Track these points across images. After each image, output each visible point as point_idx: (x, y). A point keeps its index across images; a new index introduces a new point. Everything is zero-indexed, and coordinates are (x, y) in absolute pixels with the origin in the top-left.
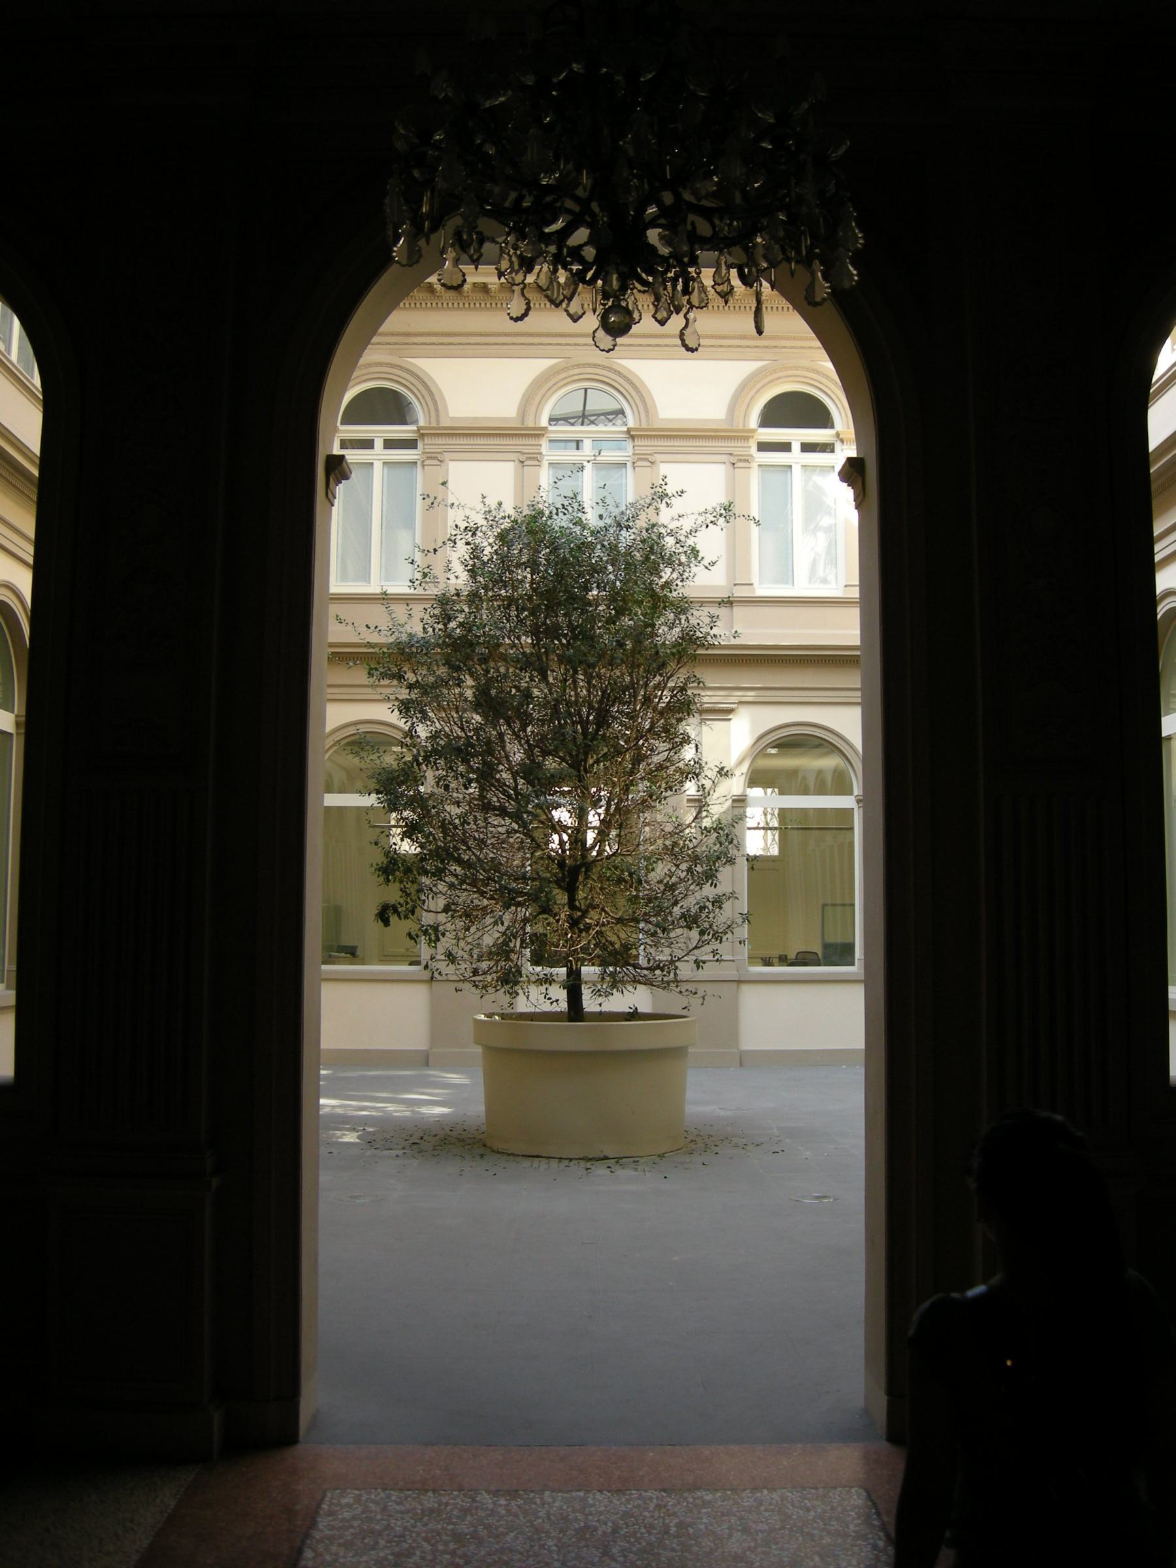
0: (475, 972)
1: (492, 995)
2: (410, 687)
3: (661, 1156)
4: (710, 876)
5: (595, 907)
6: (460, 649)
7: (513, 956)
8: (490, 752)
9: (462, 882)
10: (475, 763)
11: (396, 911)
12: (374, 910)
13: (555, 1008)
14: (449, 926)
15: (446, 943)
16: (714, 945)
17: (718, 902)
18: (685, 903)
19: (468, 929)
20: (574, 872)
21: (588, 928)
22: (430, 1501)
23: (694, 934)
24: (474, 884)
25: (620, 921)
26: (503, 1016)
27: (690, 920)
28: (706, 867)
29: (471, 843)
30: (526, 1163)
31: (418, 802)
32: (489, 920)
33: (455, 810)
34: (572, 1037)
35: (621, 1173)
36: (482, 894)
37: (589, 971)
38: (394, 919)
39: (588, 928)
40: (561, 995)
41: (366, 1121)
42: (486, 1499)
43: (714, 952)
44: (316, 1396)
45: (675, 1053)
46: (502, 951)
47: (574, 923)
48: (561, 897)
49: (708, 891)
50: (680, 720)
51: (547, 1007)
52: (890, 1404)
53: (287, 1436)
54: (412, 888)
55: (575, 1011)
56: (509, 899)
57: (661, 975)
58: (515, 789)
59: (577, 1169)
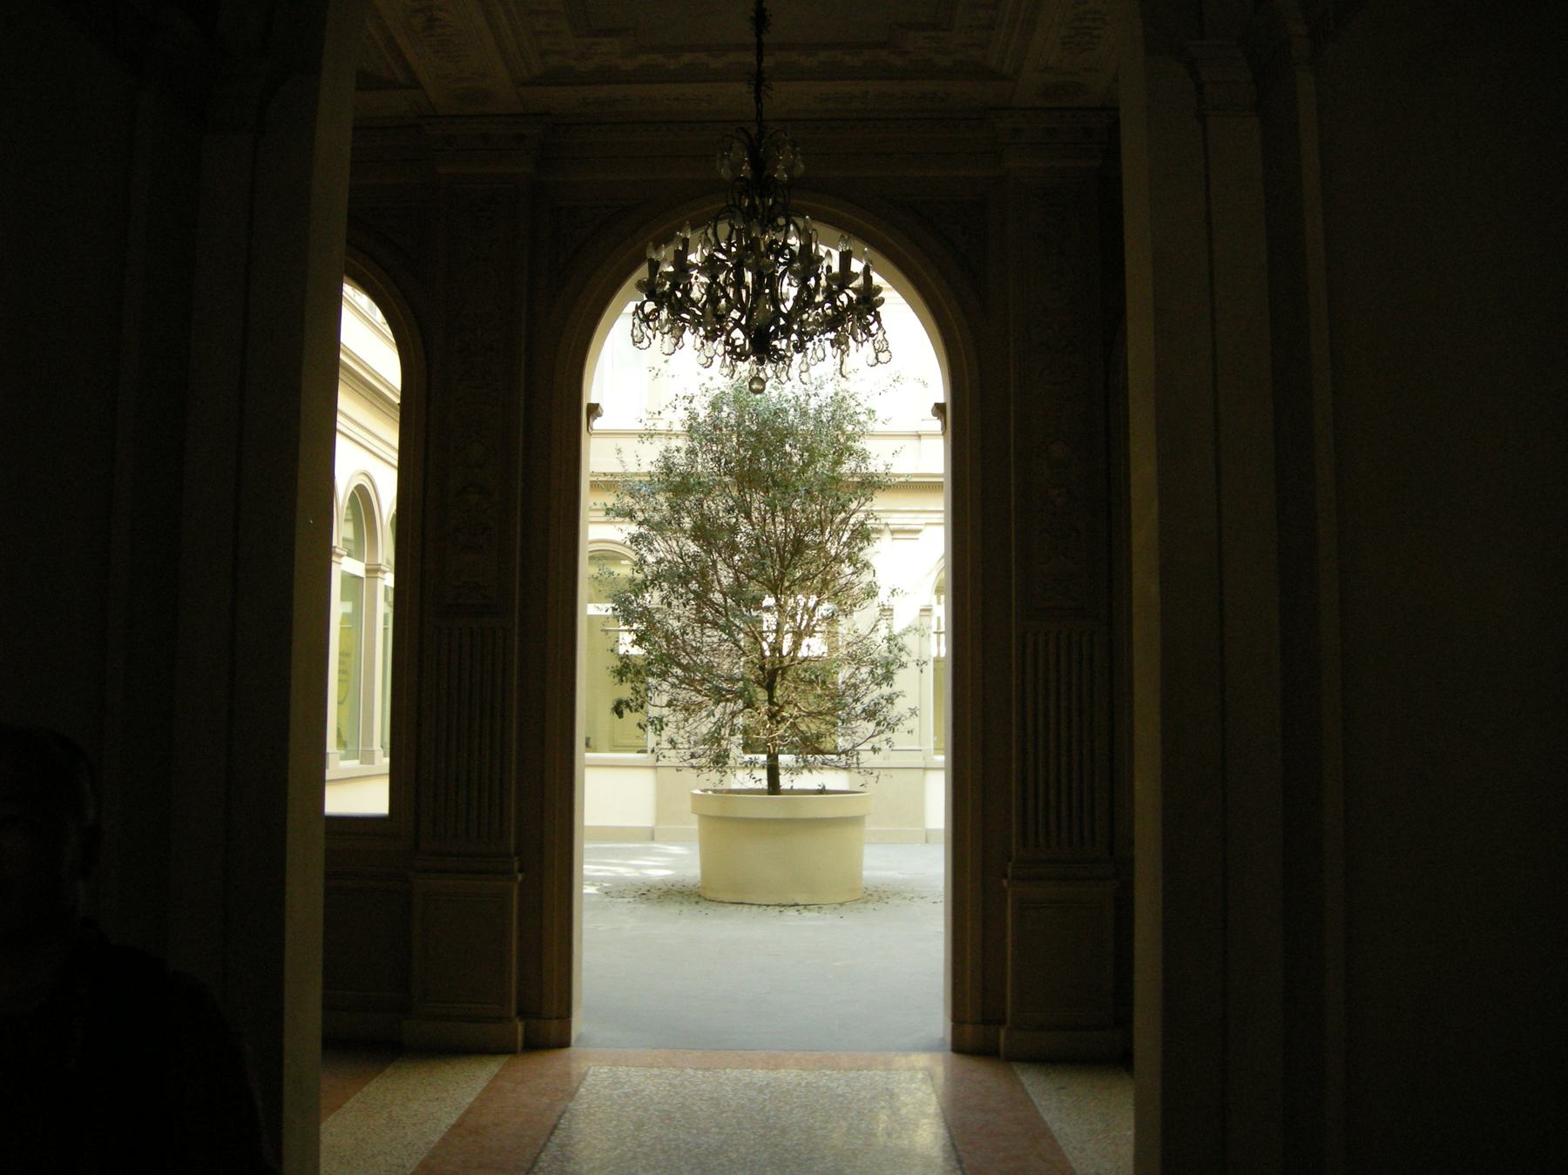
0: (693, 756)
1: (706, 774)
2: (640, 524)
3: (841, 904)
4: (888, 677)
5: (789, 703)
6: (679, 484)
7: (724, 743)
8: (704, 575)
9: (682, 682)
10: (694, 586)
11: (628, 705)
12: (610, 705)
13: (758, 786)
14: (671, 718)
15: (668, 732)
16: (888, 734)
17: (890, 700)
18: (866, 700)
19: (686, 720)
20: (772, 675)
21: (784, 719)
22: (655, 1071)
23: (871, 726)
24: (691, 682)
25: (809, 714)
26: (715, 791)
27: (870, 714)
28: (886, 672)
29: (689, 649)
30: (733, 908)
31: (646, 615)
32: (704, 714)
33: (676, 624)
34: (772, 808)
35: (806, 914)
36: (699, 692)
37: (785, 759)
38: (626, 712)
39: (784, 719)
40: (763, 775)
41: (603, 879)
42: (691, 1072)
43: (888, 741)
44: (580, 1025)
45: (856, 821)
46: (714, 738)
47: (772, 716)
48: (762, 695)
49: (885, 690)
50: (861, 549)
51: (751, 785)
52: (954, 1029)
53: (564, 1043)
54: (642, 687)
55: (774, 787)
56: (719, 696)
57: (848, 759)
58: (725, 608)
59: (774, 912)
